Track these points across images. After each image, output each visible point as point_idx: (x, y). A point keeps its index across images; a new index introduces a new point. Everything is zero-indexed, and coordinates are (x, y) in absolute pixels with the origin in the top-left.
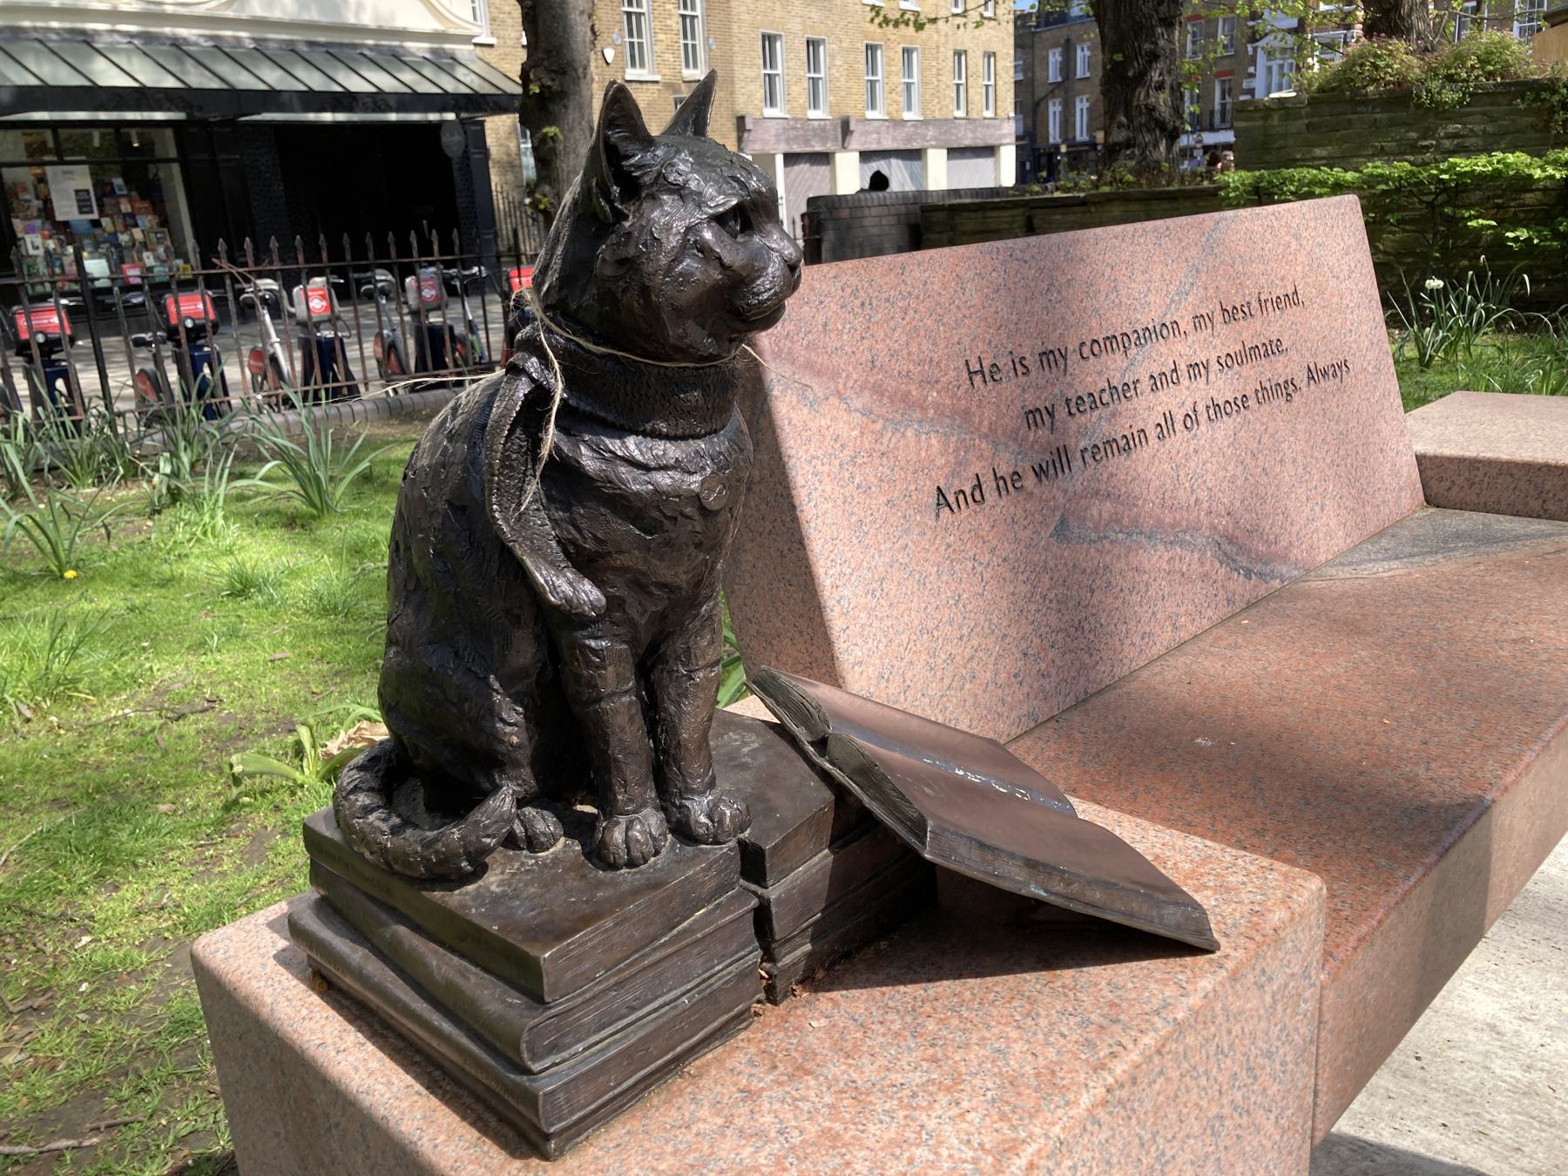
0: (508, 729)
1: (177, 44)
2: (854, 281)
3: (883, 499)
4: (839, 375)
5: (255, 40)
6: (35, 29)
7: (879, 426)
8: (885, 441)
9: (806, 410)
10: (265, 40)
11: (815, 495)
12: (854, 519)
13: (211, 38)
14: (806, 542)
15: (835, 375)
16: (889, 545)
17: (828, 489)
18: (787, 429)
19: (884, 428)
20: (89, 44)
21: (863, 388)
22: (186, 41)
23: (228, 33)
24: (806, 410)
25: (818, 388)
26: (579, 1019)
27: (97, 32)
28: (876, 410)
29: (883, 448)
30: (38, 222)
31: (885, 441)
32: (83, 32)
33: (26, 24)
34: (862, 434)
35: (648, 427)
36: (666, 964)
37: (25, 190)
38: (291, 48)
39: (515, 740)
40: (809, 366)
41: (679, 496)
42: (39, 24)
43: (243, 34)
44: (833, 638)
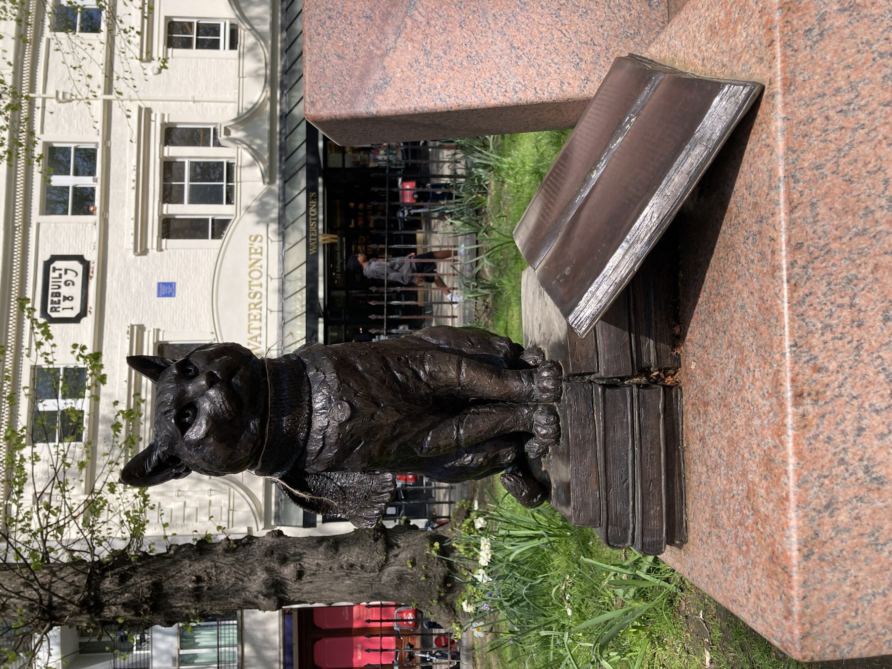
0: (475, 462)
1: (285, 72)
2: (314, 22)
3: (458, 32)
4: (371, 52)
5: (282, 31)
6: (280, 139)
7: (409, 22)
8: (420, 18)
9: (389, 89)
10: (282, 24)
11: (443, 96)
12: (465, 63)
13: (282, 54)
14: (472, 108)
15: (370, 56)
16: (490, 34)
17: (441, 81)
18: (398, 107)
19: (411, 17)
20: (287, 115)
21: (383, 33)
22: (284, 66)
23: (279, 45)
24: (389, 89)
25: (376, 77)
26: (616, 515)
27: (281, 110)
28: (398, 23)
29: (424, 23)
30: (371, 155)
31: (420, 18)
32: (281, 117)
33: (278, 143)
34: (412, 40)
35: (301, 443)
36: (610, 455)
37: (355, 158)
38: (286, 11)
39: (481, 460)
40: (362, 78)
41: (339, 434)
42: (278, 137)
43: (279, 38)
44: (540, 101)
